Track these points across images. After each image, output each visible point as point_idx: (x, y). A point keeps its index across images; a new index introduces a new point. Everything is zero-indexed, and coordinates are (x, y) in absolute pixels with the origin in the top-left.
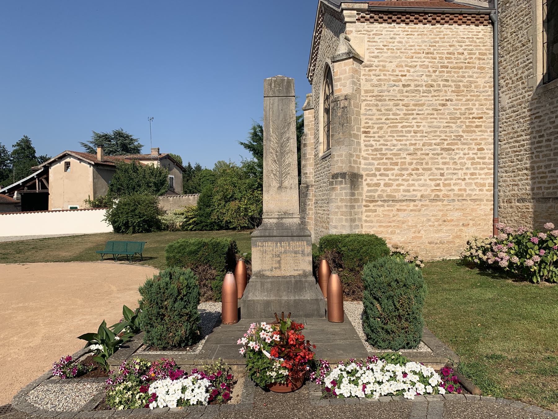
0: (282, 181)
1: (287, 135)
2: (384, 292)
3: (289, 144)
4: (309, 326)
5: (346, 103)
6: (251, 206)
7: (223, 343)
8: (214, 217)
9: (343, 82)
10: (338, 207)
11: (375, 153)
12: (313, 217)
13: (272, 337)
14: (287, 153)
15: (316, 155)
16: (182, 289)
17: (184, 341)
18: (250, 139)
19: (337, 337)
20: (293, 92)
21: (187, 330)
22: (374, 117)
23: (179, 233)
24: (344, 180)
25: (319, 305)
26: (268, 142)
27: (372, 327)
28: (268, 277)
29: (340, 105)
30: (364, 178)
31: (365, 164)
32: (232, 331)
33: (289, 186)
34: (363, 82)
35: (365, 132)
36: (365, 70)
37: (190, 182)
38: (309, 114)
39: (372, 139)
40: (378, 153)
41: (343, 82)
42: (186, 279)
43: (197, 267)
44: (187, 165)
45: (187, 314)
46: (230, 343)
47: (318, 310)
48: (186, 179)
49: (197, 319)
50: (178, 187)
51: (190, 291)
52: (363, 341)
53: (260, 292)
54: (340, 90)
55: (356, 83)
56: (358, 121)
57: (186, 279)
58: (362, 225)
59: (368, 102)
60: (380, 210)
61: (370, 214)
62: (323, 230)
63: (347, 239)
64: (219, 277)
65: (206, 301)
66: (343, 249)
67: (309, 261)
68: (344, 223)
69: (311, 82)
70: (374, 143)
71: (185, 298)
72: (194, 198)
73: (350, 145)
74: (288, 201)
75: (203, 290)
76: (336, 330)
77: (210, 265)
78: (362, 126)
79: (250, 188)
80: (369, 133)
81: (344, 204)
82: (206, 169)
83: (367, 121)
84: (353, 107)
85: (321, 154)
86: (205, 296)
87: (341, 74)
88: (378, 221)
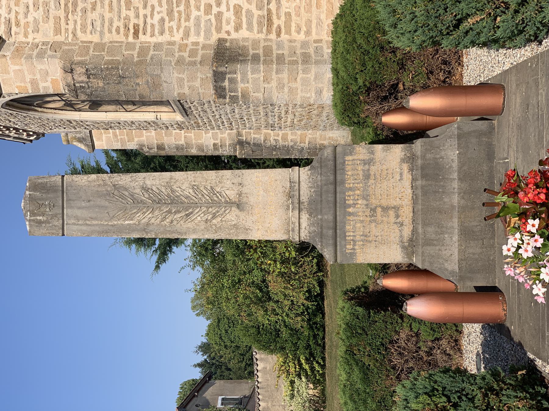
0: (226, 202)
1: (138, 191)
2: (445, 9)
3: (154, 188)
4: (512, 153)
5: (79, 70)
6: (278, 251)
7: (543, 325)
8: (299, 323)
9: (38, 76)
10: (281, 86)
11: (176, 15)
12: (299, 132)
13: (532, 235)
14: (173, 191)
15: (180, 126)
16: (436, 405)
17: (539, 402)
18: (149, 252)
19: (533, 101)
20: (53, 179)
21: (516, 397)
22: (107, 15)
23: (328, 390)
24: (228, 76)
25: (469, 133)
26: (151, 228)
27: (513, 32)
28: (414, 231)
30: (225, 36)
31: (198, 34)
32: (519, 304)
33: (236, 189)
34: (39, 38)
35: (136, 34)
36: (16, 33)
37: (231, 366)
38: (100, 139)
39: (149, 20)
40: (175, 10)
41: (38, 76)
42: (417, 397)
43: (394, 368)
44: (199, 369)
45: (485, 395)
46: (543, 311)
47: (480, 134)
48: (226, 373)
49: (495, 374)
50: (240, 390)
51: (440, 389)
52: (541, 49)
54: (54, 81)
55: (42, 51)
56: (113, 47)
57: (417, 397)
59: (78, 27)
60: (287, 5)
61: (293, 25)
62: (324, 114)
63: (342, 74)
64: (414, 324)
65: (460, 350)
66: (360, 82)
68: (311, 76)
69: (39, 135)
70: (157, 17)
71: (454, 398)
72: (262, 360)
73: (160, 64)
74: (266, 191)
75: (439, 357)
76: (518, 100)
77: (391, 342)
78: (123, 39)
79: (243, 253)
80: (138, 25)
81: (274, 76)
82: (207, 335)
83: (114, 30)
84: (87, 58)
85: (178, 117)
86: (452, 352)
87: (23, 80)
88: (309, 11)
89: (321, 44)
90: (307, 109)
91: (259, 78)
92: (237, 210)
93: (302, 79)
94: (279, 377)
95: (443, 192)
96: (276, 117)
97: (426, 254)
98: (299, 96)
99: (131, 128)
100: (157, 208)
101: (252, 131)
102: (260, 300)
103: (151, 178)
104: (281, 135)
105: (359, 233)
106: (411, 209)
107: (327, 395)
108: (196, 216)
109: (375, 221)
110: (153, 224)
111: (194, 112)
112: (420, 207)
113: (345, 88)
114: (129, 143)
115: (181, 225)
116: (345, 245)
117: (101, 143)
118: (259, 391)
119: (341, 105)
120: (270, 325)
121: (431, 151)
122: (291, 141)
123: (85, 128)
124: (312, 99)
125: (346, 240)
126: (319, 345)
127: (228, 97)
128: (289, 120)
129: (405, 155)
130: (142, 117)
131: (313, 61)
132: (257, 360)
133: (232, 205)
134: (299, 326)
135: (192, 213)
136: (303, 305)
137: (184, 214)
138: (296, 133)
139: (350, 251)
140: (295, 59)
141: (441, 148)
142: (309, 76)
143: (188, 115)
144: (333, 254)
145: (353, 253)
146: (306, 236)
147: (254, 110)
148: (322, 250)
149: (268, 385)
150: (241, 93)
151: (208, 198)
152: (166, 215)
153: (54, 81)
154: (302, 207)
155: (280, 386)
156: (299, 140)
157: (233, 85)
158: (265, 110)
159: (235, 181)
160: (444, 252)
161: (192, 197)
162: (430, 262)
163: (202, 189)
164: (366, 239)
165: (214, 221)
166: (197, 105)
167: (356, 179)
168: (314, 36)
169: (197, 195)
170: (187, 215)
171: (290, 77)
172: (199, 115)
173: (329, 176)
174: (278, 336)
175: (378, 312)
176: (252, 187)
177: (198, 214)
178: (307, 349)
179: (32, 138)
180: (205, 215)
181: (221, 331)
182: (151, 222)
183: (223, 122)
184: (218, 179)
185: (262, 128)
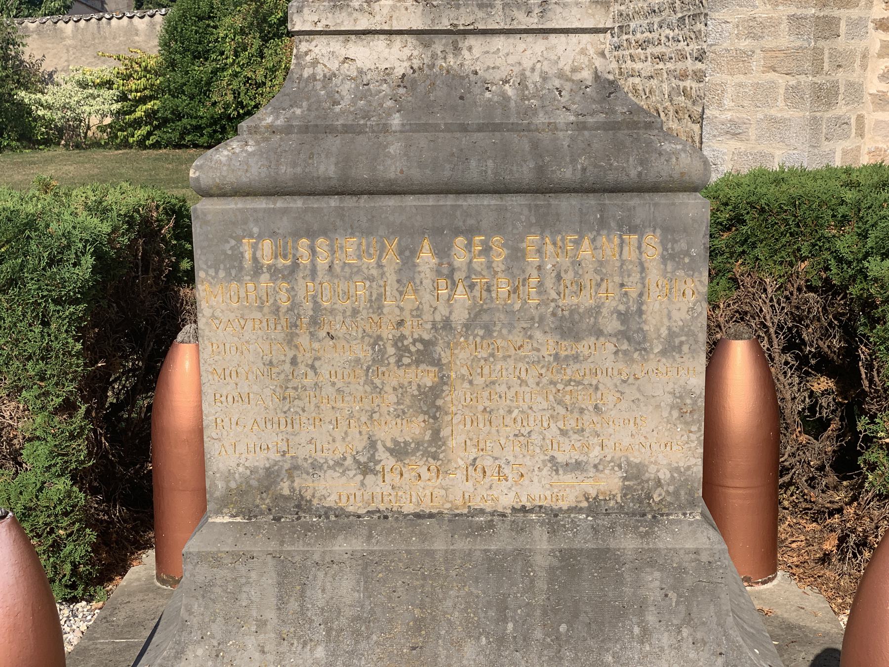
10: (754, 29)
23: (98, 154)
28: (339, 520)
53: (269, 637)
58: (860, 118)
67: (680, 396)
68: (780, 110)
72: (152, 25)
89: (853, 135)
93: (773, 85)
94: (119, 59)
95: (501, 640)
96: (647, 34)
97: (243, 570)
102: (264, 20)
105: (327, 293)
106: (427, 507)
107: (88, 152)
109: (379, 359)
112: (439, 545)
113: (842, 210)
116: (273, 234)
118: (93, 20)
119: (783, 199)
120: (216, 41)
121: (674, 588)
124: (716, 113)
125: (296, 235)
126: (182, 138)
128: (638, 66)
129: (659, 483)
131: (818, 114)
132: (152, 16)
134: (215, 98)
139: (248, 255)
140: (826, 66)
141: (685, 632)
142: (781, 103)
144: (231, 178)
145: (241, 268)
146: (315, 63)
149: (105, 38)
155: (104, 62)
158: (667, 5)
160: (251, 642)
162: (211, 584)
164: (300, 324)
167: (559, 278)
168: (873, 116)
171: (781, 55)
173: (574, 161)
174: (195, 57)
175: (79, 329)
178: (172, 113)
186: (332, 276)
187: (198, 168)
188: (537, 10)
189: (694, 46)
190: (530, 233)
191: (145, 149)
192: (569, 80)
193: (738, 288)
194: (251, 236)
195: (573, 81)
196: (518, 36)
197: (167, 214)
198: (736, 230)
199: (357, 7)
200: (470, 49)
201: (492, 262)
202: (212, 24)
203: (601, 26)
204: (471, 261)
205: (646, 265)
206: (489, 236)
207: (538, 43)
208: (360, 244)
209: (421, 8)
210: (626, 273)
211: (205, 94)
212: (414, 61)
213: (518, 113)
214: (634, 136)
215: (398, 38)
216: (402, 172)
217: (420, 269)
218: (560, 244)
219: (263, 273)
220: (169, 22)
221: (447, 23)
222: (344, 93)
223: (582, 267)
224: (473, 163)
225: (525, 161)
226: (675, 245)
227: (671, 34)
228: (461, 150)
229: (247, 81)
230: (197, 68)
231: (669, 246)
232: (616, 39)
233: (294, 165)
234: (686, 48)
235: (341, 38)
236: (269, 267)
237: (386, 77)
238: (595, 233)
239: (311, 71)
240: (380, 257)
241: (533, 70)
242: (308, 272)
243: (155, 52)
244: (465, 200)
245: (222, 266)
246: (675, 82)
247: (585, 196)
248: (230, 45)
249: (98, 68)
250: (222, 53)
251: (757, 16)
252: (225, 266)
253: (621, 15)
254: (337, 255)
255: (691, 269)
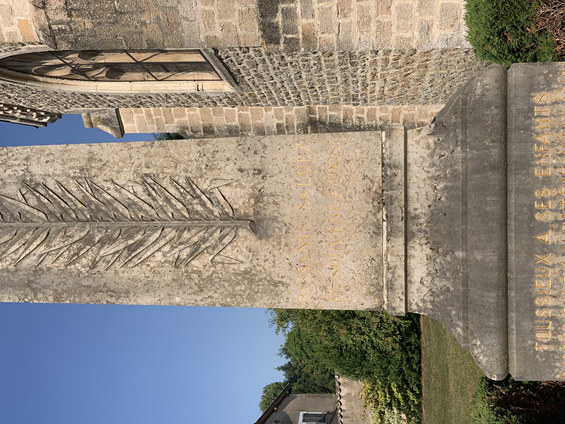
0: (225, 217)
1: (12, 190)
3: (51, 184)
8: (389, 344)
12: (390, 107)
14: (95, 189)
15: (232, 101)
26: (44, 279)
29: (61, 22)
33: (249, 183)
38: (130, 120)
44: (282, 373)
54: (23, 24)
62: (427, 78)
72: (345, 384)
85: (226, 87)
90: (402, 69)
91: (330, 8)
92: (252, 237)
94: (366, 406)
96: (359, 84)
98: (393, 37)
99: (169, 105)
100: (59, 231)
101: (328, 106)
103: (43, 159)
104: (366, 112)
108: (152, 250)
110: (49, 269)
111: (246, 78)
114: (167, 125)
115: (116, 272)
116: (533, 332)
117: (132, 125)
119: (490, 6)
120: (355, 345)
122: (380, 119)
123: (109, 106)
125: (533, 317)
126: (414, 370)
127: (282, 41)
128: (377, 88)
130: (178, 88)
133: (238, 223)
134: (390, 348)
135: (141, 243)
136: (395, 323)
137: (122, 246)
138: (386, 108)
139: (546, 348)
143: (238, 84)
144: (497, 355)
145: (554, 352)
146: (423, 301)
147: (328, 74)
148: (466, 340)
149: (353, 414)
150: (303, 34)
151: (179, 206)
152: (80, 249)
153: (23, 24)
154: (414, 228)
155: (367, 416)
156: (390, 118)
157: (289, 22)
158: (343, 73)
159: (247, 164)
161: (141, 203)
163: (165, 183)
165: (195, 263)
166: (248, 67)
169: (154, 199)
170: (131, 249)
172: (254, 83)
173: (487, 148)
174: (365, 359)
176: (289, 180)
177: (157, 246)
179: (45, 120)
180: (173, 248)
181: (302, 341)
182: (44, 266)
183: (287, 94)
184: (205, 159)
185: (341, 102)
186: (559, 296)
187: (491, 375)
188: (394, 171)
189: (369, 56)
190: (533, 173)
191: (422, 394)
192: (434, 151)
193: (545, 29)
194: (534, 345)
195: (435, 148)
196: (408, 181)
197: (492, 390)
198: (507, 32)
199: (392, 275)
200: (415, 209)
201: (551, 196)
202: (345, 348)
203: (403, 133)
204: (551, 210)
205: (554, 101)
206: (535, 199)
207: (413, 169)
208: (539, 278)
209: (392, 238)
210: (559, 113)
211: (387, 354)
212: (423, 242)
213: (455, 181)
214: (471, 111)
215: (409, 251)
216: (493, 252)
217: (555, 242)
218: (540, 155)
219: (557, 339)
220: (344, 374)
221: (401, 223)
222: (442, 284)
223: (555, 141)
224: (488, 209)
225: (487, 177)
226: (541, 83)
227: (360, 69)
228: (480, 216)
229: (379, 328)
230: (371, 359)
231: (541, 87)
232: (360, 102)
233: (489, 317)
234: (369, 60)
235: (409, 285)
236: (554, 335)
237: (432, 259)
238: (533, 133)
239: (428, 304)
240: (548, 266)
241: (428, 172)
242: (557, 311)
243: (361, 384)
244: (512, 213)
245: (553, 364)
246: (390, 66)
247: (509, 140)
248: (357, 337)
249: (371, 420)
250: (362, 342)
251: (356, 21)
252: (553, 362)
253: (346, 100)
254: (546, 293)
255: (556, 72)
